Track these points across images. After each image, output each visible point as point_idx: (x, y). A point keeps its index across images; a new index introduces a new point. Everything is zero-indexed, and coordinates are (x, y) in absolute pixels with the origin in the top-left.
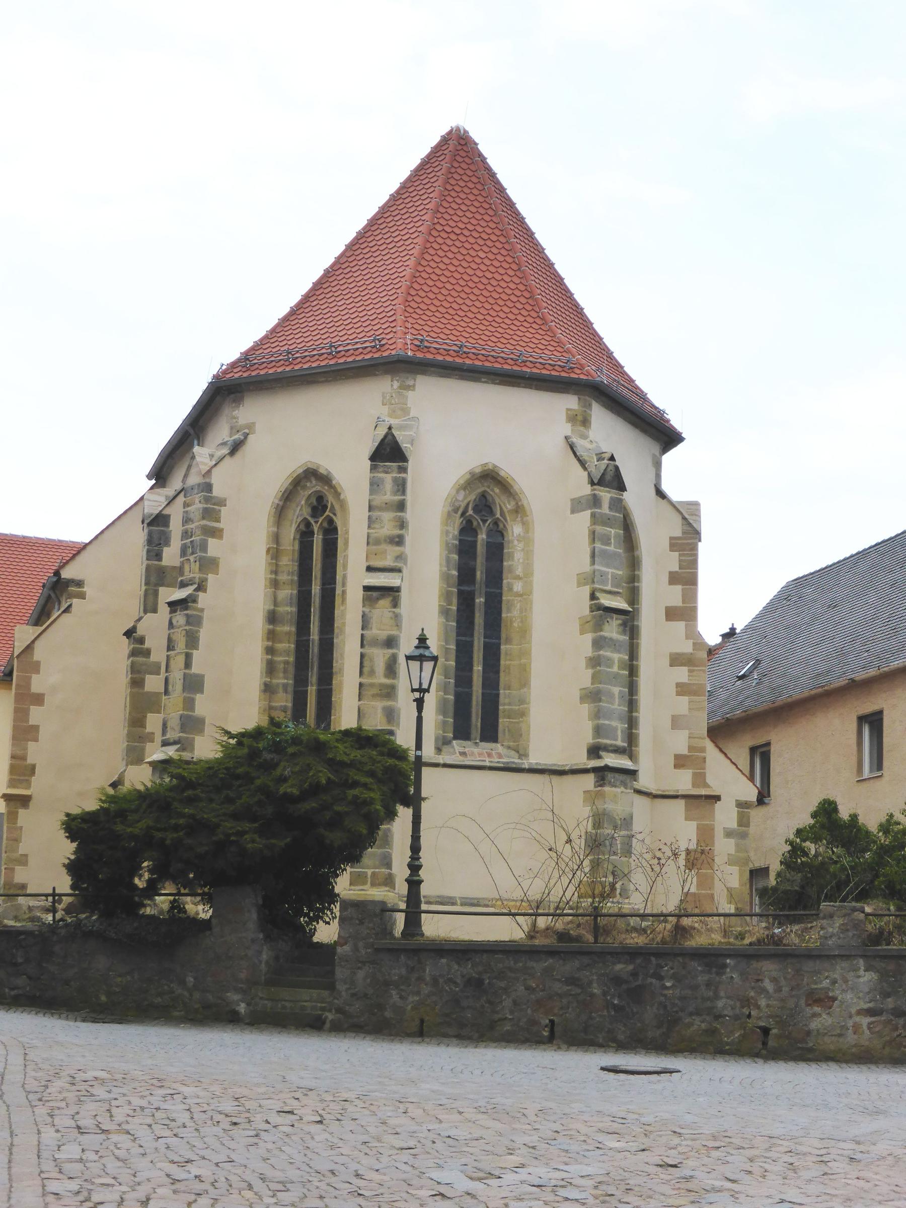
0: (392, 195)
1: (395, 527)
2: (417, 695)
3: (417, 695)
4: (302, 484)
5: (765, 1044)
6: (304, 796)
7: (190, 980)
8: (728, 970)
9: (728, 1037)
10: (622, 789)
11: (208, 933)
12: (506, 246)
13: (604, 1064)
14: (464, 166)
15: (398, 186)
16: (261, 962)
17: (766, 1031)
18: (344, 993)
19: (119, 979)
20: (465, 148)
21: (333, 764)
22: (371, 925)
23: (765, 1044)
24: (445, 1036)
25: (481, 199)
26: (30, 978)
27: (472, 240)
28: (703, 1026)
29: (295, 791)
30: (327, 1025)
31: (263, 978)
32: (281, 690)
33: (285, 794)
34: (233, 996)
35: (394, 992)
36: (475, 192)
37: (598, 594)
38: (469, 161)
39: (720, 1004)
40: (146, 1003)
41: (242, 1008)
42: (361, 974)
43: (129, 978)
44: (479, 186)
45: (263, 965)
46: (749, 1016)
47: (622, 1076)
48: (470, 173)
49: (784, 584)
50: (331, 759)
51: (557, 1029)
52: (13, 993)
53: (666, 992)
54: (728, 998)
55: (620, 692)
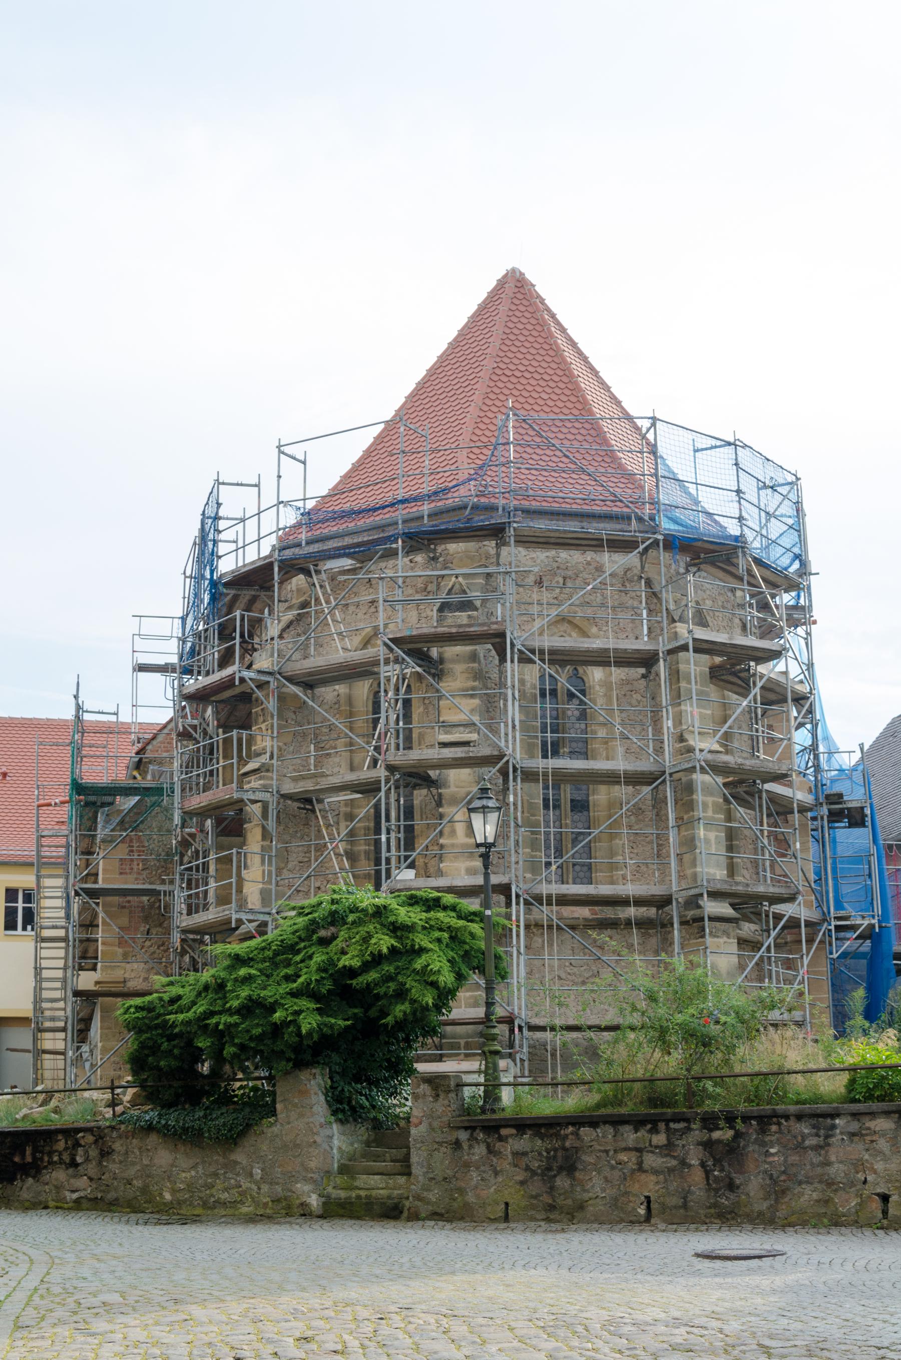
0: (450, 344)
1: (468, 679)
2: (482, 850)
3: (482, 850)
4: (372, 642)
5: (885, 1213)
6: (366, 967)
7: (257, 1172)
8: (838, 1131)
9: (844, 1207)
10: (725, 939)
11: (272, 1120)
12: (569, 386)
13: (700, 1248)
14: (522, 308)
15: (455, 333)
16: (332, 1148)
17: (885, 1198)
18: (421, 1178)
19: (184, 1175)
20: (521, 290)
21: (396, 929)
22: (446, 1102)
23: (885, 1213)
24: (533, 1219)
25: (540, 340)
26: (91, 1179)
27: (534, 382)
28: (815, 1196)
29: (356, 963)
30: (405, 1214)
31: (336, 1165)
32: (363, 857)
33: (345, 967)
34: (301, 1187)
35: (474, 1174)
36: (535, 333)
37: (686, 736)
38: (527, 303)
39: (832, 1170)
40: (213, 1199)
41: (314, 1201)
42: (438, 1156)
43: (193, 1173)
44: (538, 328)
45: (335, 1151)
46: (865, 1182)
47: (718, 1264)
48: (529, 315)
49: (889, 721)
50: (393, 923)
51: (654, 1206)
52: (75, 1196)
53: (771, 1159)
54: (841, 1162)
55: (717, 837)
